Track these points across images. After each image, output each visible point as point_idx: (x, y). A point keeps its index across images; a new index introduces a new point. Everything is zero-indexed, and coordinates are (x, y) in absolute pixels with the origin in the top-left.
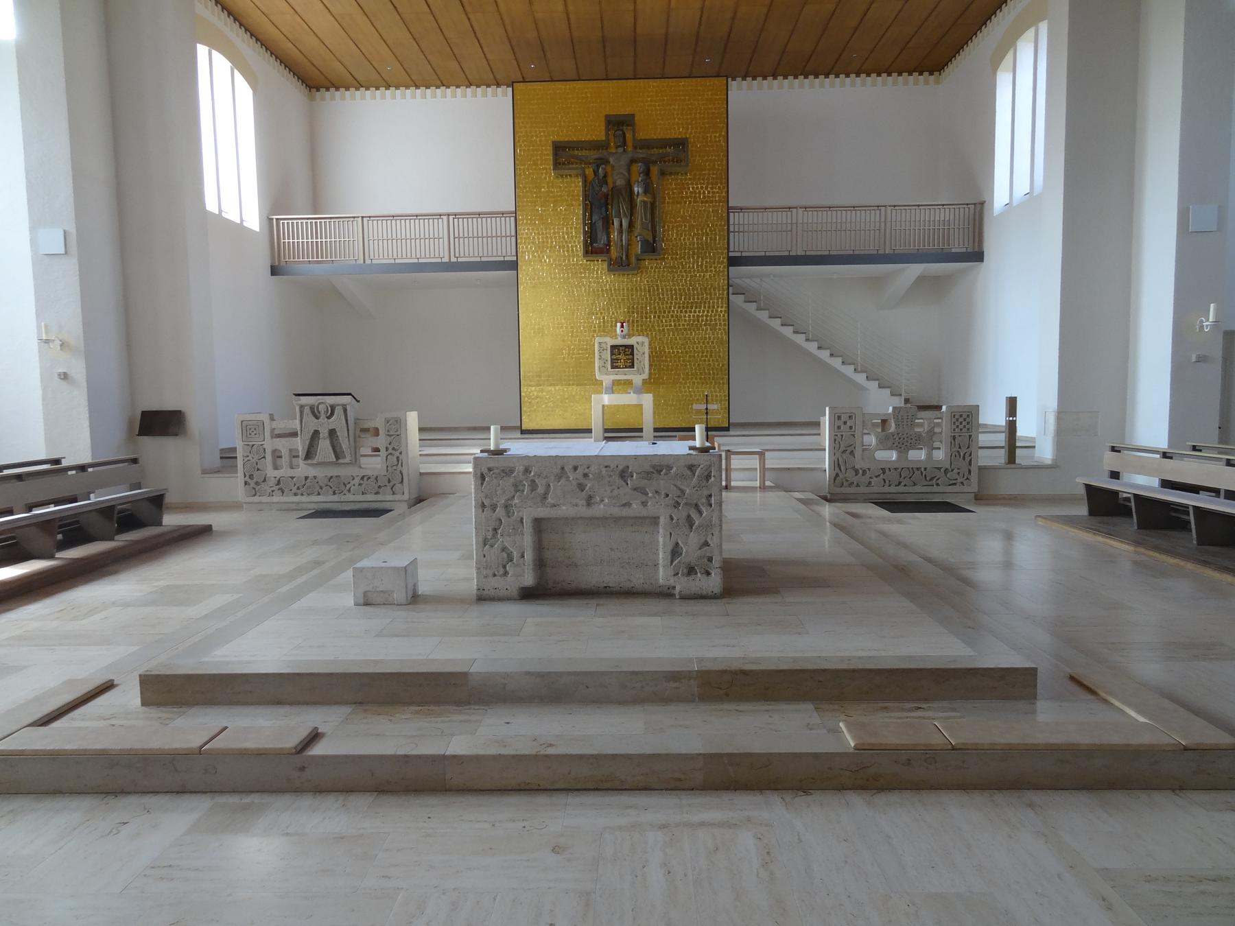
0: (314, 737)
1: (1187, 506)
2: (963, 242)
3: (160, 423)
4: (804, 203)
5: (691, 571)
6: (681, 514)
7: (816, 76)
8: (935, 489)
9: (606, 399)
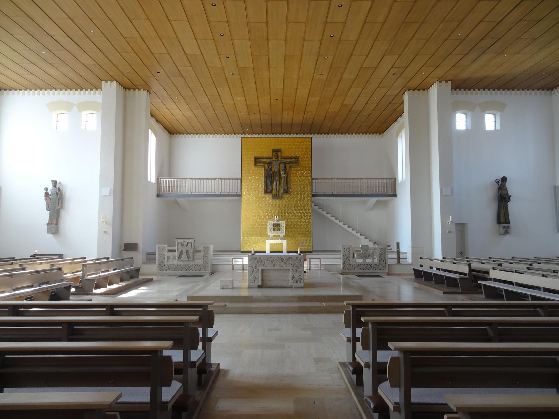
0: (120, 396)
1: (527, 295)
2: (390, 192)
3: (131, 247)
4: (337, 177)
5: (297, 282)
6: (295, 268)
7: (342, 134)
8: (375, 271)
9: (272, 242)
